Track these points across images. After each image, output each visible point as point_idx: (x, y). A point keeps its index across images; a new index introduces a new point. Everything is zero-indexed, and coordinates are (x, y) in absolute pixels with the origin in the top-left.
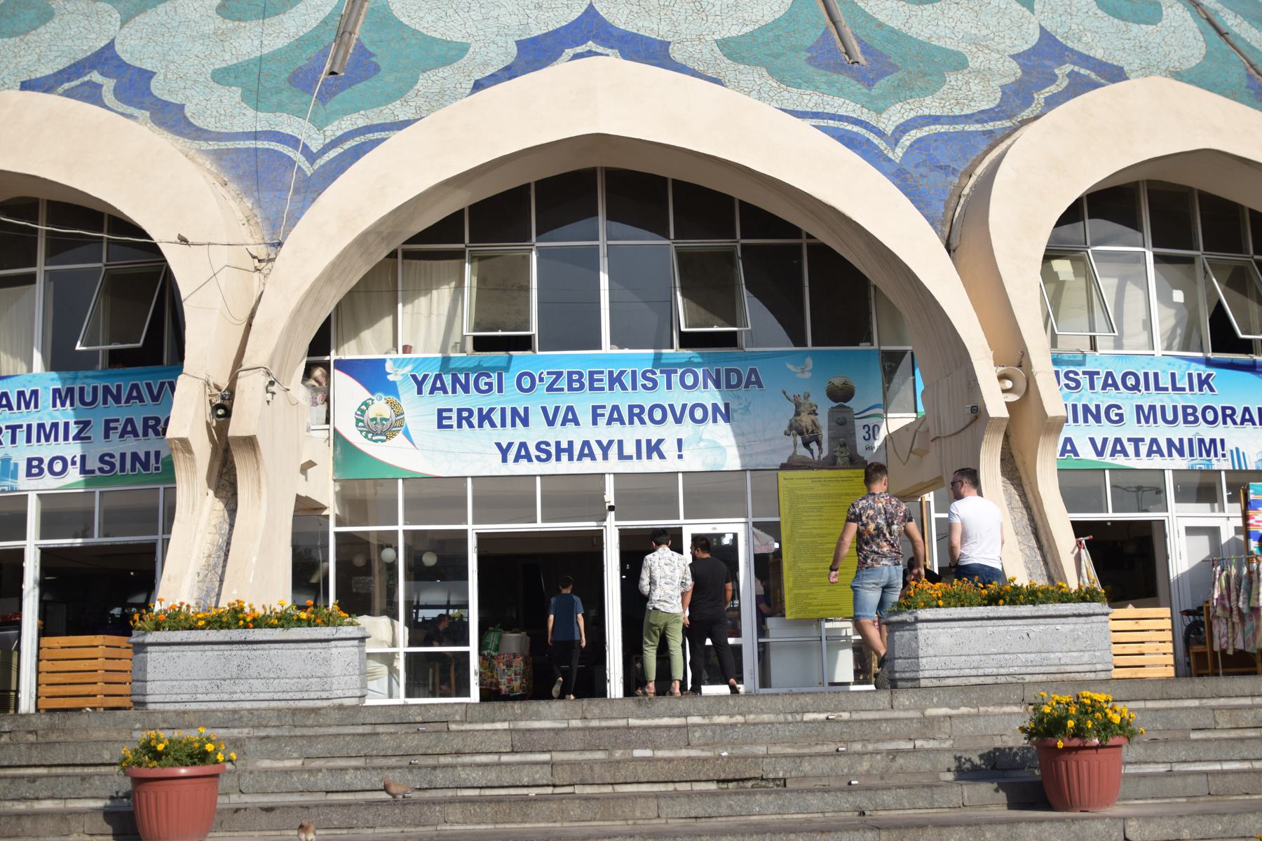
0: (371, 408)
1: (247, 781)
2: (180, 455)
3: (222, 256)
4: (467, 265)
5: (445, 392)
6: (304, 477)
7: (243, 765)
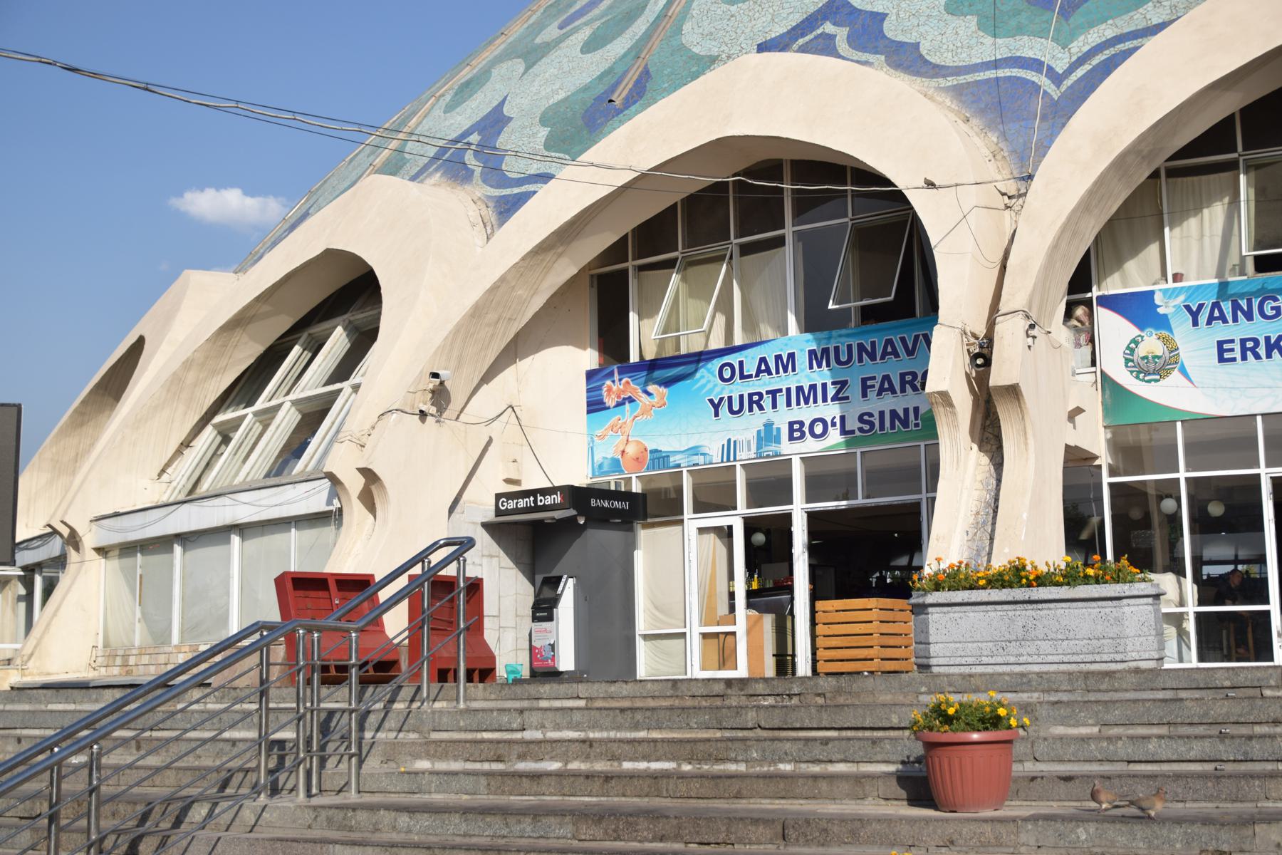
0: (1141, 346)
1: (1041, 748)
2: (941, 409)
3: (971, 196)
4: (1242, 176)
5: (1225, 321)
6: (1072, 425)
7: (1035, 731)
